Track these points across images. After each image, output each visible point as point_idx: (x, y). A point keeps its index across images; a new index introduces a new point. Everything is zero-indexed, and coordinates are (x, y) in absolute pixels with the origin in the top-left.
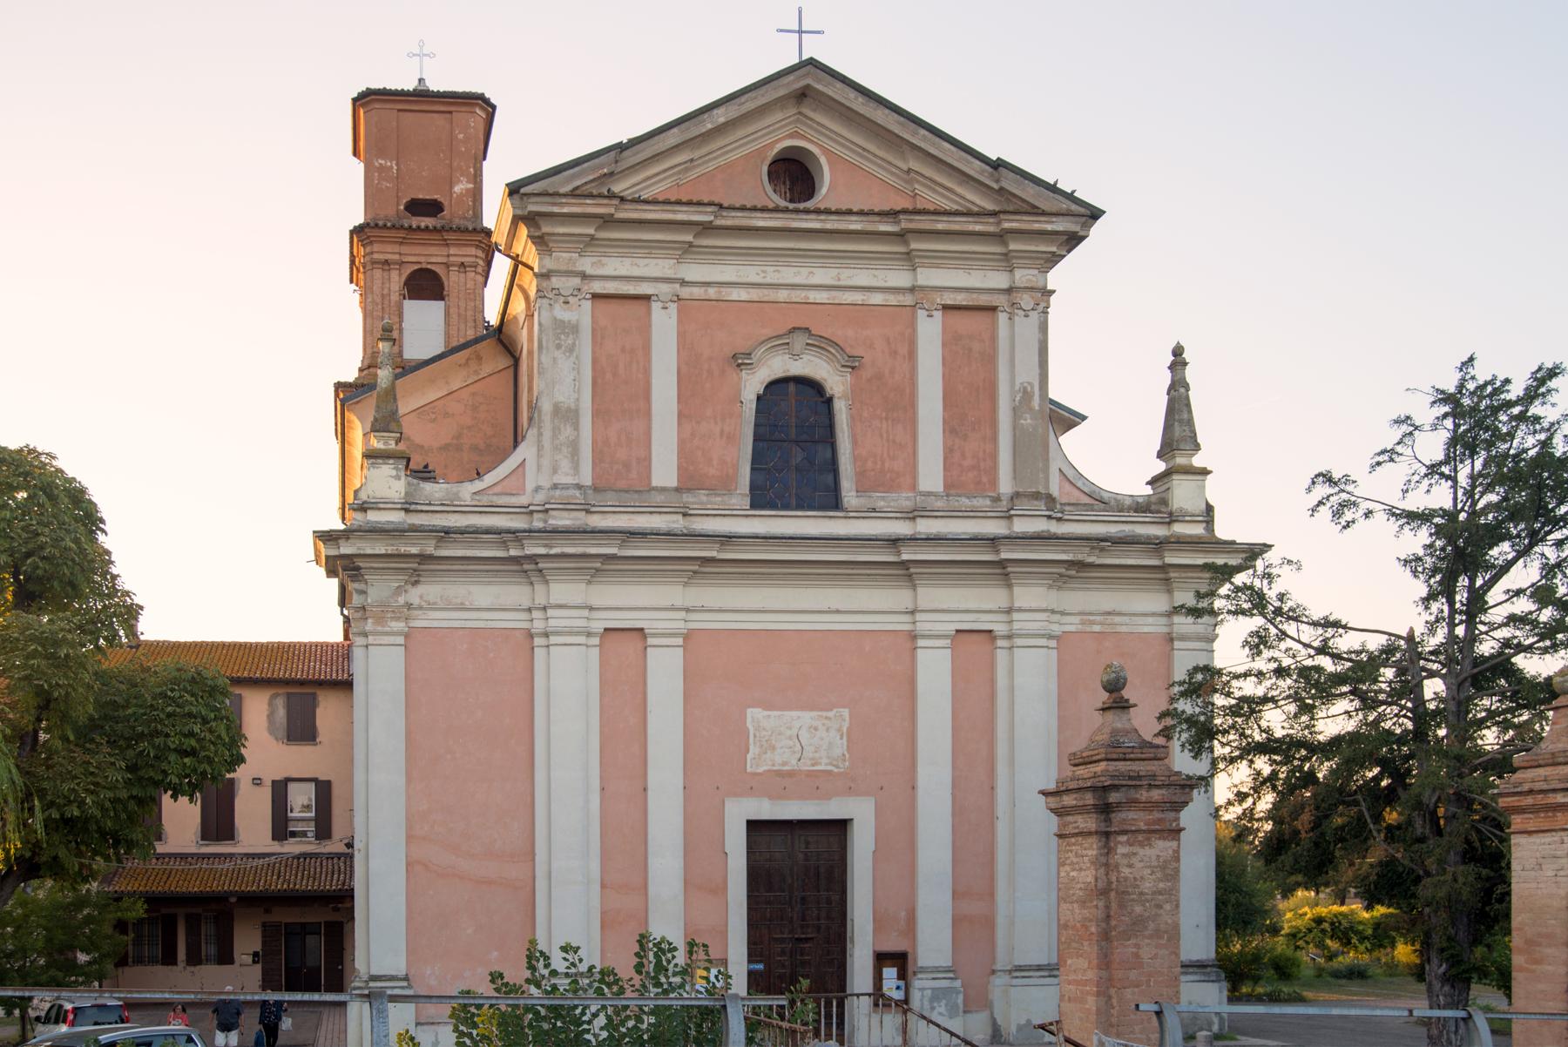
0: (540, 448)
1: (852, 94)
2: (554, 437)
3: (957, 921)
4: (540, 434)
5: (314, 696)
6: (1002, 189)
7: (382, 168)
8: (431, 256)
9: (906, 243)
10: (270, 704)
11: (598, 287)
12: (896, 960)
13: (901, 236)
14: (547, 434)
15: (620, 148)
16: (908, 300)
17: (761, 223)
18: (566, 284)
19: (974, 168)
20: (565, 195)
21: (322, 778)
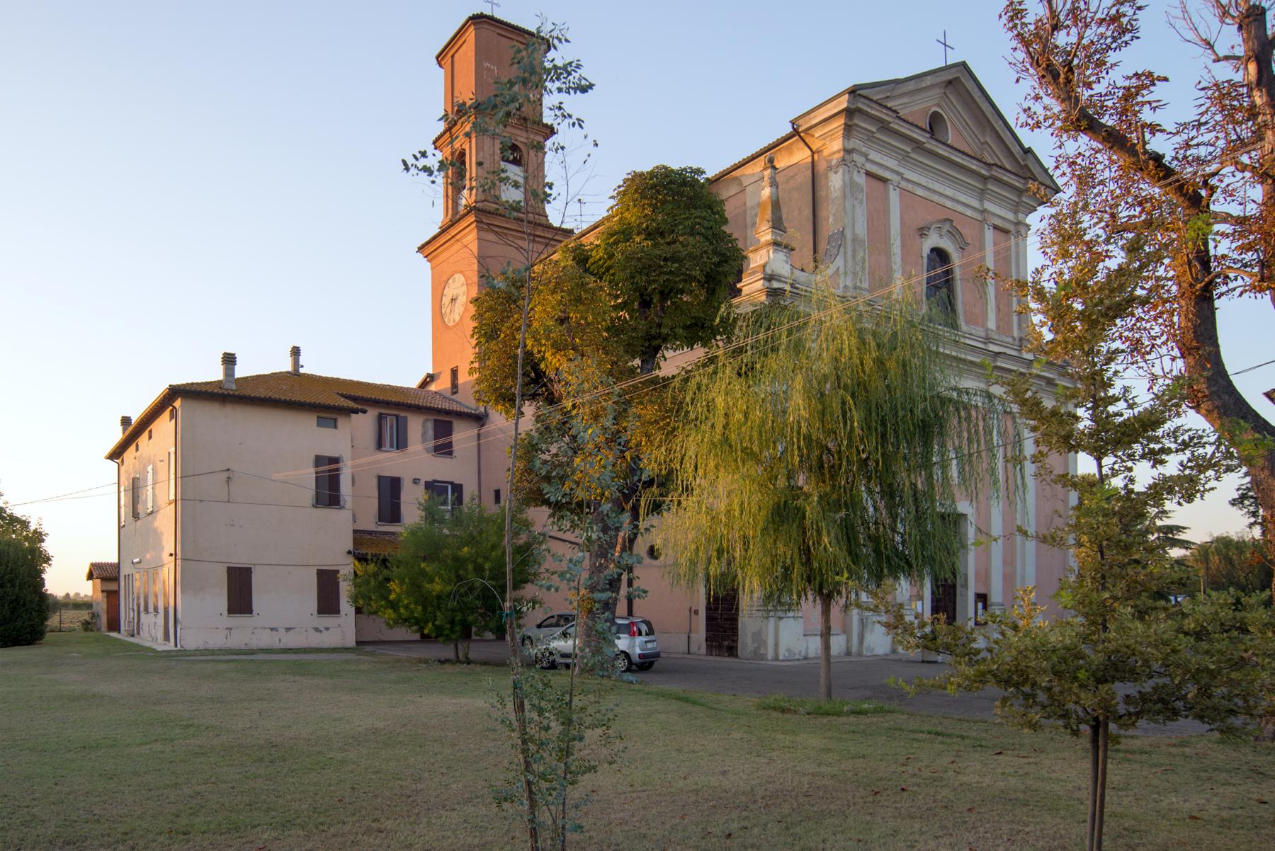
0: (845, 261)
1: (976, 90)
2: (854, 256)
3: (1004, 576)
4: (845, 253)
5: (450, 423)
6: (1026, 166)
7: (488, 69)
8: (521, 138)
9: (985, 184)
10: (423, 426)
11: (869, 167)
12: (982, 598)
13: (985, 179)
14: (850, 253)
15: (897, 82)
16: (979, 217)
17: (941, 152)
18: (859, 159)
19: (1016, 149)
20: (876, 102)
21: (456, 482)
